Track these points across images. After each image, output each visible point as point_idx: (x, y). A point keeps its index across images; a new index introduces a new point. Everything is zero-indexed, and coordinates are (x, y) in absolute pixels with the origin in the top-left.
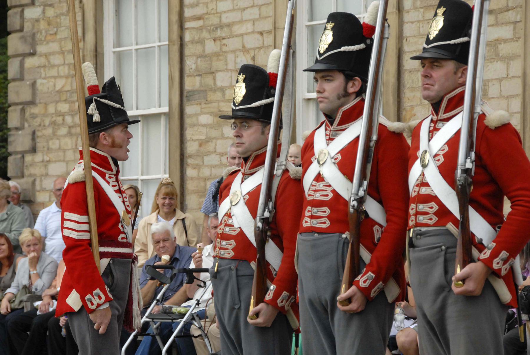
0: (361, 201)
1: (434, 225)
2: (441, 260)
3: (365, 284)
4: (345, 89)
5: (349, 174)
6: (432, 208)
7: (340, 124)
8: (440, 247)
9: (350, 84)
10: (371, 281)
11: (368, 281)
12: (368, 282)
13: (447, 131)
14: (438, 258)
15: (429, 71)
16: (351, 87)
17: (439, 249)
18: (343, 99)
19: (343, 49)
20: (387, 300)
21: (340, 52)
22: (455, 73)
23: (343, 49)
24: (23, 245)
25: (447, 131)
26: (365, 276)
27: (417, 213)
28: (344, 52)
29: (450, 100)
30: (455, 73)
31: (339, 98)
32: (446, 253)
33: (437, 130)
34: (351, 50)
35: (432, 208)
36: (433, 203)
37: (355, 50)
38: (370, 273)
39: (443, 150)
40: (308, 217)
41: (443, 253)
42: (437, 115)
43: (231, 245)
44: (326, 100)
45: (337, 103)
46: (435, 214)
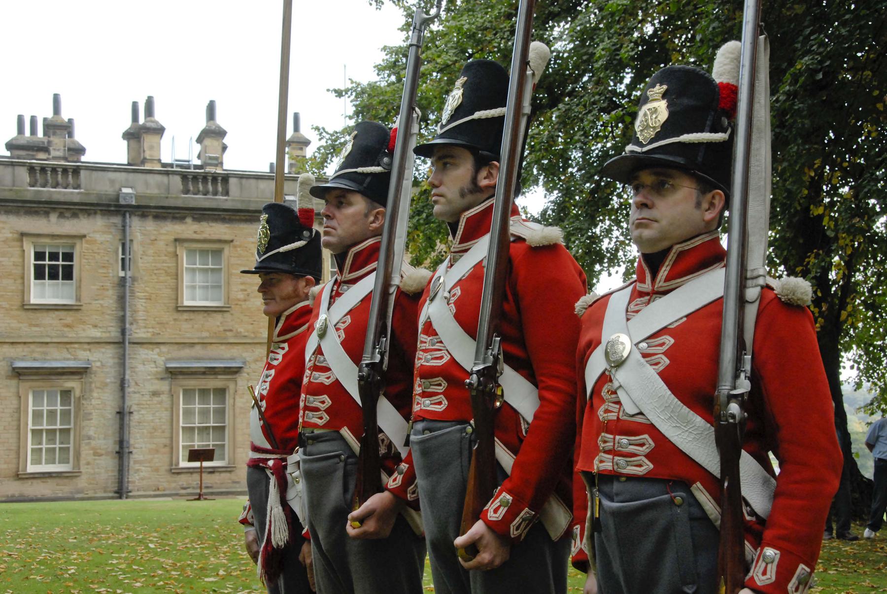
0: (490, 374)
1: (324, 427)
2: (340, 474)
3: (497, 515)
4: (474, 180)
5: (471, 330)
6: (323, 402)
7: (463, 240)
8: (338, 456)
9: (484, 173)
10: (506, 509)
11: (502, 508)
12: (503, 511)
13: (354, 295)
14: (335, 471)
15: (332, 209)
16: (485, 178)
17: (337, 460)
18: (469, 198)
19: (477, 115)
20: (550, 537)
21: (473, 120)
22: (366, 216)
23: (477, 115)
24: (869, 424)
25: (354, 295)
26: (498, 500)
27: (306, 408)
28: (479, 120)
29: (357, 255)
30: (366, 216)
31: (463, 195)
32: (346, 465)
33: (339, 294)
34: (490, 116)
35: (323, 402)
36: (326, 396)
37: (496, 115)
38: (504, 494)
39: (344, 323)
40: (419, 395)
41: (342, 464)
42: (342, 275)
43: (642, 445)
44: (442, 199)
45: (459, 202)
46: (327, 411)
